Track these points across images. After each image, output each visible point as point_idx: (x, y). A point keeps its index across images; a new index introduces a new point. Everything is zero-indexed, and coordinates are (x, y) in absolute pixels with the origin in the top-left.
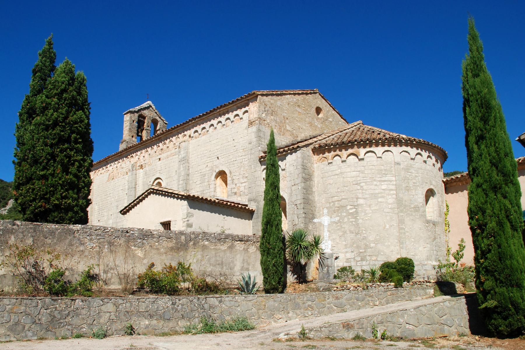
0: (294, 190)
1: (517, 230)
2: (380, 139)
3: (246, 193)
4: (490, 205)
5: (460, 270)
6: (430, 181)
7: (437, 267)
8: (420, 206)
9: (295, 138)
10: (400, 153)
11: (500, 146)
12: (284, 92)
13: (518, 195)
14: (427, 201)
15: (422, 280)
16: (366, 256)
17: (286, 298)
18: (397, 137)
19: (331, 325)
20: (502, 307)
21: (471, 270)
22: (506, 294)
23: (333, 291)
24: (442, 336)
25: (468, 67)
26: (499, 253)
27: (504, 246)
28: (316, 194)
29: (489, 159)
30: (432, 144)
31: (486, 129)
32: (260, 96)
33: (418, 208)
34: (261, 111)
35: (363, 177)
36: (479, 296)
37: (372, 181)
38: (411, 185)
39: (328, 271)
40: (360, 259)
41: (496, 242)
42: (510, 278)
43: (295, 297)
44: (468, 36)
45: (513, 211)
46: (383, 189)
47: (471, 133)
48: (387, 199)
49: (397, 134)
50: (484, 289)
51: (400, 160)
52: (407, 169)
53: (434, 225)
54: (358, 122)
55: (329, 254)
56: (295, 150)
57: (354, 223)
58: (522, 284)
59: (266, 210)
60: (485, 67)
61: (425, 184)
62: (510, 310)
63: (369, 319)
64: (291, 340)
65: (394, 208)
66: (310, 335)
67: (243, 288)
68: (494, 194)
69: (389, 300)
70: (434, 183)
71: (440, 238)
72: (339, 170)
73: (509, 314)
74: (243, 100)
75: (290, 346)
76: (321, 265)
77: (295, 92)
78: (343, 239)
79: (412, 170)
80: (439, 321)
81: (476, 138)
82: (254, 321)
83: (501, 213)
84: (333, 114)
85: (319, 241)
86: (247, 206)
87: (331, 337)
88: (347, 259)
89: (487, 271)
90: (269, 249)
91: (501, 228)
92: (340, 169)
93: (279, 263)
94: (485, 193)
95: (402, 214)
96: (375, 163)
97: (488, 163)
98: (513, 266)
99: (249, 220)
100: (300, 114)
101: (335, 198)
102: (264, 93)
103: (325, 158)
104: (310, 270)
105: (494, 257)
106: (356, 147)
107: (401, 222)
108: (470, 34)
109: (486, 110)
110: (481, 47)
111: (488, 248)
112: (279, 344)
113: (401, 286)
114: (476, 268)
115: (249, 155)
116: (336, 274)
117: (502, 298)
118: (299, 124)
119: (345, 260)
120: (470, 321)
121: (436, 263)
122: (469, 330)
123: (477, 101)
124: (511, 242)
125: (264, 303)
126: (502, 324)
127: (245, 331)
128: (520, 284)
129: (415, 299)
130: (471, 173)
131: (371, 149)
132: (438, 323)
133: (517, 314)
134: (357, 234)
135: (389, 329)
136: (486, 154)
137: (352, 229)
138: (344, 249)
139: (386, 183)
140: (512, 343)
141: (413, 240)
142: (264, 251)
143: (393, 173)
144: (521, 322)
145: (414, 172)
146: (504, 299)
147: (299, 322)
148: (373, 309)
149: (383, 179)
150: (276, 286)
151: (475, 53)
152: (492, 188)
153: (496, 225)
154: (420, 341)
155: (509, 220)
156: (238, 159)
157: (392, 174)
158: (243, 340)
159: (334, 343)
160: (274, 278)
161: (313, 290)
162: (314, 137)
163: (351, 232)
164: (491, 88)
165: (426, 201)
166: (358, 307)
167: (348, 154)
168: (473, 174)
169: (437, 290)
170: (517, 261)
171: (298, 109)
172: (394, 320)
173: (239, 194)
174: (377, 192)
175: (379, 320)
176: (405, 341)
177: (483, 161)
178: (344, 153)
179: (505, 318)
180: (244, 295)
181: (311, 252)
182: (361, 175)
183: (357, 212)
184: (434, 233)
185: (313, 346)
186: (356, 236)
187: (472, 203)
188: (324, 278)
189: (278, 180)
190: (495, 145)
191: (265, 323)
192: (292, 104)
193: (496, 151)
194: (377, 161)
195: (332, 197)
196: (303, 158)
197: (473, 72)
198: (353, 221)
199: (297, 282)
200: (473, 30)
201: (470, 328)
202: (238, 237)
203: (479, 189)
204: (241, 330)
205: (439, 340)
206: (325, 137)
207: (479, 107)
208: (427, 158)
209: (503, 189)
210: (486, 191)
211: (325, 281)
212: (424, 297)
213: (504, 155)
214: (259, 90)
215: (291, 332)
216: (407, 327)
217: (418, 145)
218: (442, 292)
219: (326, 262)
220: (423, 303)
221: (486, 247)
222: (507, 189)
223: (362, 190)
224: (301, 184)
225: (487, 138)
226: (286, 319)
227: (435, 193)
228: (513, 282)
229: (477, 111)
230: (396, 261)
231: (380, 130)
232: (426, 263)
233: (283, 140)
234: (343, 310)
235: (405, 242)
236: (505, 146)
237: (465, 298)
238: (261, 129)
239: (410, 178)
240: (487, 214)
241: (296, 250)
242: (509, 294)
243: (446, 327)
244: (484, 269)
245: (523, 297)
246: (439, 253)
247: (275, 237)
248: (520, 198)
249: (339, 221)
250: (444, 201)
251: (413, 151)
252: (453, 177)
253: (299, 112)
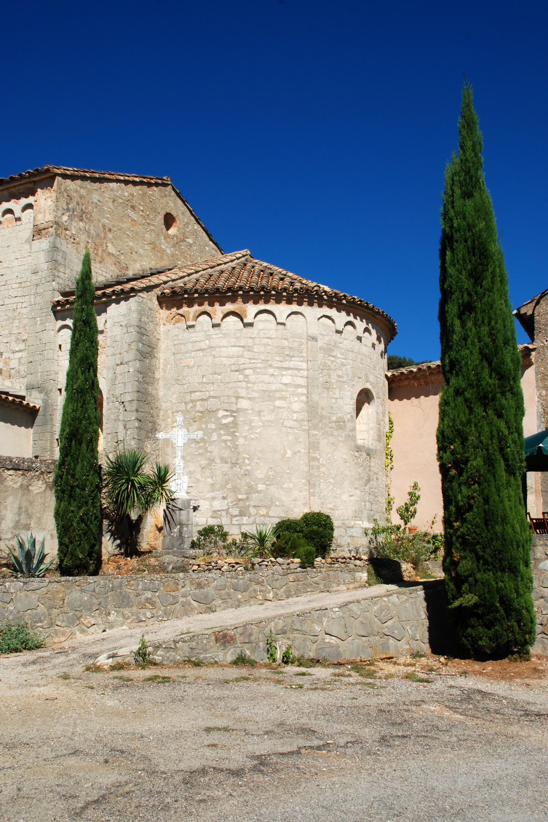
0: (121, 374)
1: (514, 474)
2: (285, 289)
3: (22, 373)
4: (475, 427)
5: (408, 538)
7: (370, 532)
8: (346, 420)
9: (124, 272)
10: (319, 319)
11: (498, 326)
12: (107, 176)
13: (520, 413)
14: (358, 410)
15: (347, 555)
16: (249, 506)
17: (105, 586)
18: (316, 288)
19: (194, 636)
20: (485, 605)
21: (426, 539)
22: (493, 583)
23: (191, 571)
24: (384, 657)
25: (456, 178)
26: (485, 511)
27: (494, 501)
28: (161, 383)
29: (478, 347)
30: (373, 307)
31: (476, 294)
32: (60, 178)
33: (344, 422)
34: (60, 208)
35: (250, 359)
36: (449, 586)
37: (265, 368)
38: (333, 381)
39: (180, 532)
40: (237, 513)
41: (482, 492)
42: (501, 556)
43: (121, 583)
44: (460, 120)
45: (510, 440)
47: (451, 297)
48: (291, 403)
49: (314, 284)
50: (457, 574)
51: (316, 333)
52: (328, 350)
53: (368, 454)
54: (244, 252)
55: (183, 501)
56: (125, 295)
58: (517, 566)
59: (70, 411)
60: (483, 182)
61: (357, 379)
62: (497, 611)
63: (261, 625)
64: (119, 667)
65: (302, 420)
66: (155, 657)
67: (19, 564)
68: (483, 408)
69: (290, 591)
70: (371, 378)
71: (377, 479)
72: (207, 342)
73: (496, 619)
74: (23, 181)
75: (121, 678)
76: (169, 522)
77: (127, 178)
78: (208, 472)
80: (380, 631)
81: (459, 308)
82: (41, 632)
83: (492, 443)
84: (195, 231)
85: (165, 475)
86: (23, 398)
87: (193, 659)
89: (465, 543)
90: (72, 487)
91: (490, 468)
92: (209, 340)
93: (92, 516)
94: (468, 407)
96: (273, 334)
97: (476, 355)
98: (506, 536)
99: (27, 427)
100: (134, 223)
101: (198, 393)
102: (68, 172)
103: (182, 316)
104: (145, 530)
105: (477, 519)
106: (240, 300)
107: (313, 446)
108: (464, 117)
109: (480, 258)
110: (480, 144)
111: (468, 503)
112: (99, 675)
113: (312, 565)
114: (445, 536)
115: (33, 297)
116: (195, 539)
117: (486, 590)
118: (131, 244)
119: (210, 514)
120: (430, 629)
121: (370, 525)
122: (428, 646)
123: (466, 241)
124: (504, 493)
125: (61, 595)
126: (483, 636)
127: (25, 651)
128: (515, 567)
129: (335, 589)
130: (447, 368)
131: (268, 307)
132: (378, 633)
133: (508, 618)
134: (234, 464)
135: (296, 643)
136: (474, 337)
137: (226, 455)
138: (209, 492)
139: (290, 372)
140: (498, 668)
141: (332, 480)
142: (63, 492)
143: (304, 355)
144: (513, 632)
145: (339, 356)
146: (489, 592)
147: (129, 632)
149: (286, 364)
150: (84, 561)
151: (469, 154)
152: (480, 398)
153: (482, 464)
154: (349, 667)
155: (503, 456)
156: (7, 301)
157: (302, 357)
158: (24, 670)
159: (202, 671)
160: (80, 544)
161: (153, 570)
162: (159, 273)
163: (224, 461)
164: (490, 220)
165: (357, 410)
166: (236, 603)
168: (450, 371)
170: (513, 527)
171: (130, 212)
172: (305, 628)
173: (7, 374)
174: (273, 387)
175: (280, 626)
176: (324, 666)
177: (469, 349)
178: (218, 310)
179: (489, 625)
180: (22, 579)
181: (151, 496)
183: (235, 424)
184: (368, 469)
185: (164, 678)
186: (232, 468)
187: (446, 422)
189: (95, 354)
190: (489, 323)
191: (63, 634)
192: (121, 201)
193: (491, 335)
194: (276, 330)
195: (191, 392)
196: (141, 313)
197: (463, 188)
198: (227, 440)
199: (122, 554)
200: (470, 110)
201: (430, 643)
202: (11, 462)
203: (459, 398)
204: (16, 650)
205: (381, 664)
206: (181, 274)
207: (469, 252)
208: (364, 333)
209: (498, 402)
210: (471, 403)
211: (174, 552)
212: (351, 586)
213: (503, 343)
214: (58, 163)
215: (121, 652)
216: (327, 640)
217: (351, 307)
218: (381, 578)
219: (177, 515)
221: (465, 500)
222: (504, 401)
224: (134, 362)
225: (477, 310)
226: (103, 627)
227: (373, 398)
228: (505, 563)
229: (464, 260)
230: (302, 519)
231: (284, 272)
232: (352, 523)
233: (100, 272)
234: (210, 608)
235: (319, 485)
236: (504, 327)
237: (424, 589)
238: (59, 246)
239: (332, 367)
240: (469, 442)
241: (124, 490)
242: (497, 583)
243: (391, 641)
244: (460, 540)
245: (518, 588)
246: (374, 507)
247: (85, 463)
248: (522, 419)
249: (203, 440)
250: (387, 412)
251: (341, 318)
252: (404, 370)
253: (133, 220)
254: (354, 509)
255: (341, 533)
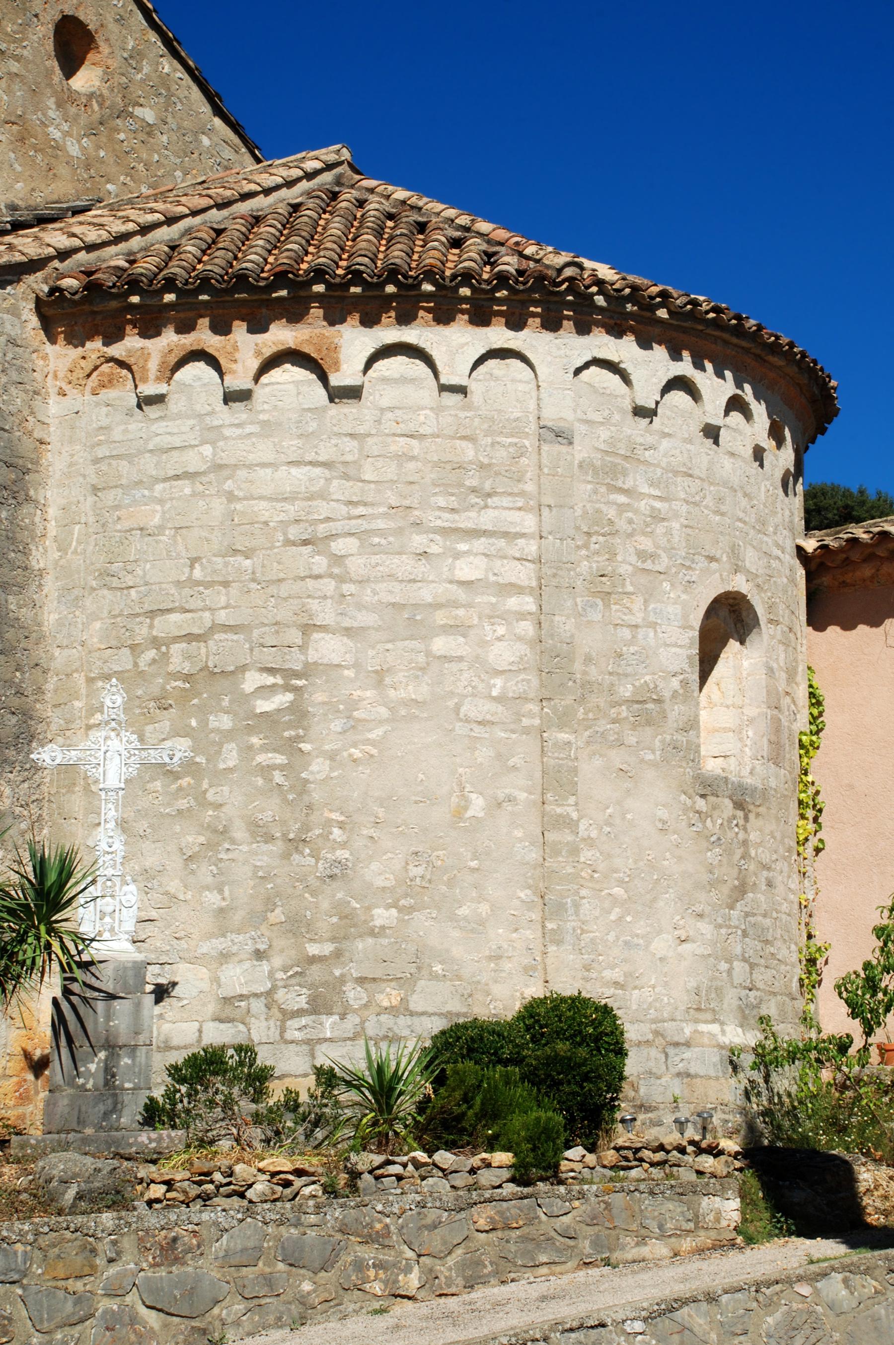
2: (467, 277)
6: (734, 552)
7: (748, 1059)
8: (667, 694)
10: (578, 371)
15: (671, 1138)
16: (342, 980)
18: (569, 272)
23: (141, 1205)
28: (50, 585)
30: (760, 327)
33: (659, 701)
35: (350, 503)
37: (399, 531)
39: (109, 1072)
40: (302, 1002)
46: (461, 583)
48: (483, 644)
49: (564, 257)
51: (569, 415)
53: (739, 805)
54: (329, 154)
55: (122, 970)
57: (278, 777)
61: (702, 563)
65: (522, 698)
69: (479, 1263)
70: (751, 559)
71: (770, 884)
72: (207, 450)
78: (205, 872)
79: (636, 480)
84: (165, 80)
85: (61, 884)
88: (227, 1000)
92: (213, 443)
95: (564, 736)
96: (427, 422)
101: (174, 617)
103: (122, 364)
106: (316, 312)
116: (158, 1093)
119: (211, 1008)
131: (410, 335)
134: (296, 844)
137: (267, 816)
138: (211, 936)
139: (481, 544)
141: (617, 891)
143: (530, 487)
145: (645, 489)
148: (385, 1321)
149: (466, 520)
157: (522, 494)
162: (42, 221)
165: (702, 661)
166: (295, 1309)
167: (268, 352)
169: (753, 1203)
174: (426, 594)
182: (339, 489)
184: (739, 852)
186: (286, 856)
188: (81, 1122)
194: (438, 410)
195: (152, 614)
198: (272, 767)
208: (727, 413)
211: (85, 1141)
212: (687, 1244)
217: (685, 331)
220: (685, 1279)
223: (341, 579)
227: (756, 622)
230: (520, 1018)
231: (464, 220)
232: (688, 1030)
235: (577, 906)
239: (622, 525)
246: (761, 977)
249: (190, 766)
250: (801, 668)
252: (859, 532)
254: (692, 984)
255: (652, 1064)
